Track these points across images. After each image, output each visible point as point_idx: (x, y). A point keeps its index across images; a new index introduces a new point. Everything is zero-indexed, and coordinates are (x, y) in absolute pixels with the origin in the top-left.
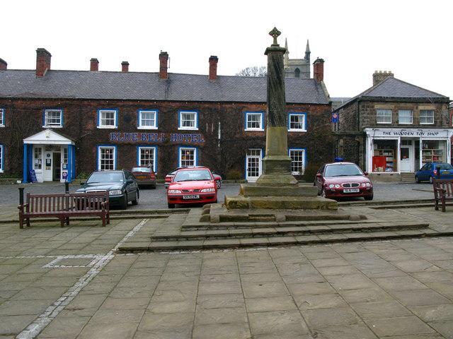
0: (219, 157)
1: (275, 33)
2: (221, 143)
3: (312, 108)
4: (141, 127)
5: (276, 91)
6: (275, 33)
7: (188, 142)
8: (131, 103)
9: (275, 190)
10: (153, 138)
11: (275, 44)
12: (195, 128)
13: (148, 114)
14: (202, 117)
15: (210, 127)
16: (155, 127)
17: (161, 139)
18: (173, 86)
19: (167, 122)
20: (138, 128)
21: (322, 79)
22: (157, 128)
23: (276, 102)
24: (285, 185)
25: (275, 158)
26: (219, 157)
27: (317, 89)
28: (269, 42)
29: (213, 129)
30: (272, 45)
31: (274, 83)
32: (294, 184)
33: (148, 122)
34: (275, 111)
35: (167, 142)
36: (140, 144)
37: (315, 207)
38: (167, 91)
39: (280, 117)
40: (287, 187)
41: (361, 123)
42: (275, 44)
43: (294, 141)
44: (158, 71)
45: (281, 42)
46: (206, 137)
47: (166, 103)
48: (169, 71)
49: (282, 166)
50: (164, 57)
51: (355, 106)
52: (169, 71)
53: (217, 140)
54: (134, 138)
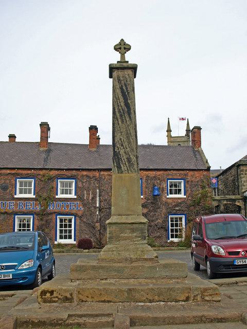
0: (98, 225)
1: (123, 47)
2: (100, 210)
3: (191, 173)
4: (18, 196)
5: (122, 122)
6: (123, 47)
7: (67, 210)
8: (8, 171)
9: (118, 270)
10: (31, 207)
11: (123, 61)
12: (73, 196)
13: (26, 183)
14: (80, 185)
15: (88, 194)
16: (32, 196)
17: (38, 208)
18: (52, 154)
19: (46, 195)
20: (15, 196)
21: (200, 146)
22: (34, 197)
23: (124, 138)
24: (137, 260)
25: (123, 219)
26: (98, 225)
27: (195, 155)
28: (115, 58)
29: (91, 196)
30: (118, 62)
31: (120, 112)
32: (151, 260)
33: (25, 191)
34: (122, 152)
35: (44, 210)
36: (16, 214)
37: (183, 298)
38: (46, 160)
39: (129, 160)
40: (140, 264)
41: (240, 188)
42: (123, 61)
43: (151, 191)
44: (39, 140)
45: (130, 58)
46: (84, 205)
47: (44, 171)
48: (50, 140)
49: (133, 231)
50: (45, 127)
51: (233, 171)
52: (50, 140)
53: (95, 207)
54: (11, 206)
